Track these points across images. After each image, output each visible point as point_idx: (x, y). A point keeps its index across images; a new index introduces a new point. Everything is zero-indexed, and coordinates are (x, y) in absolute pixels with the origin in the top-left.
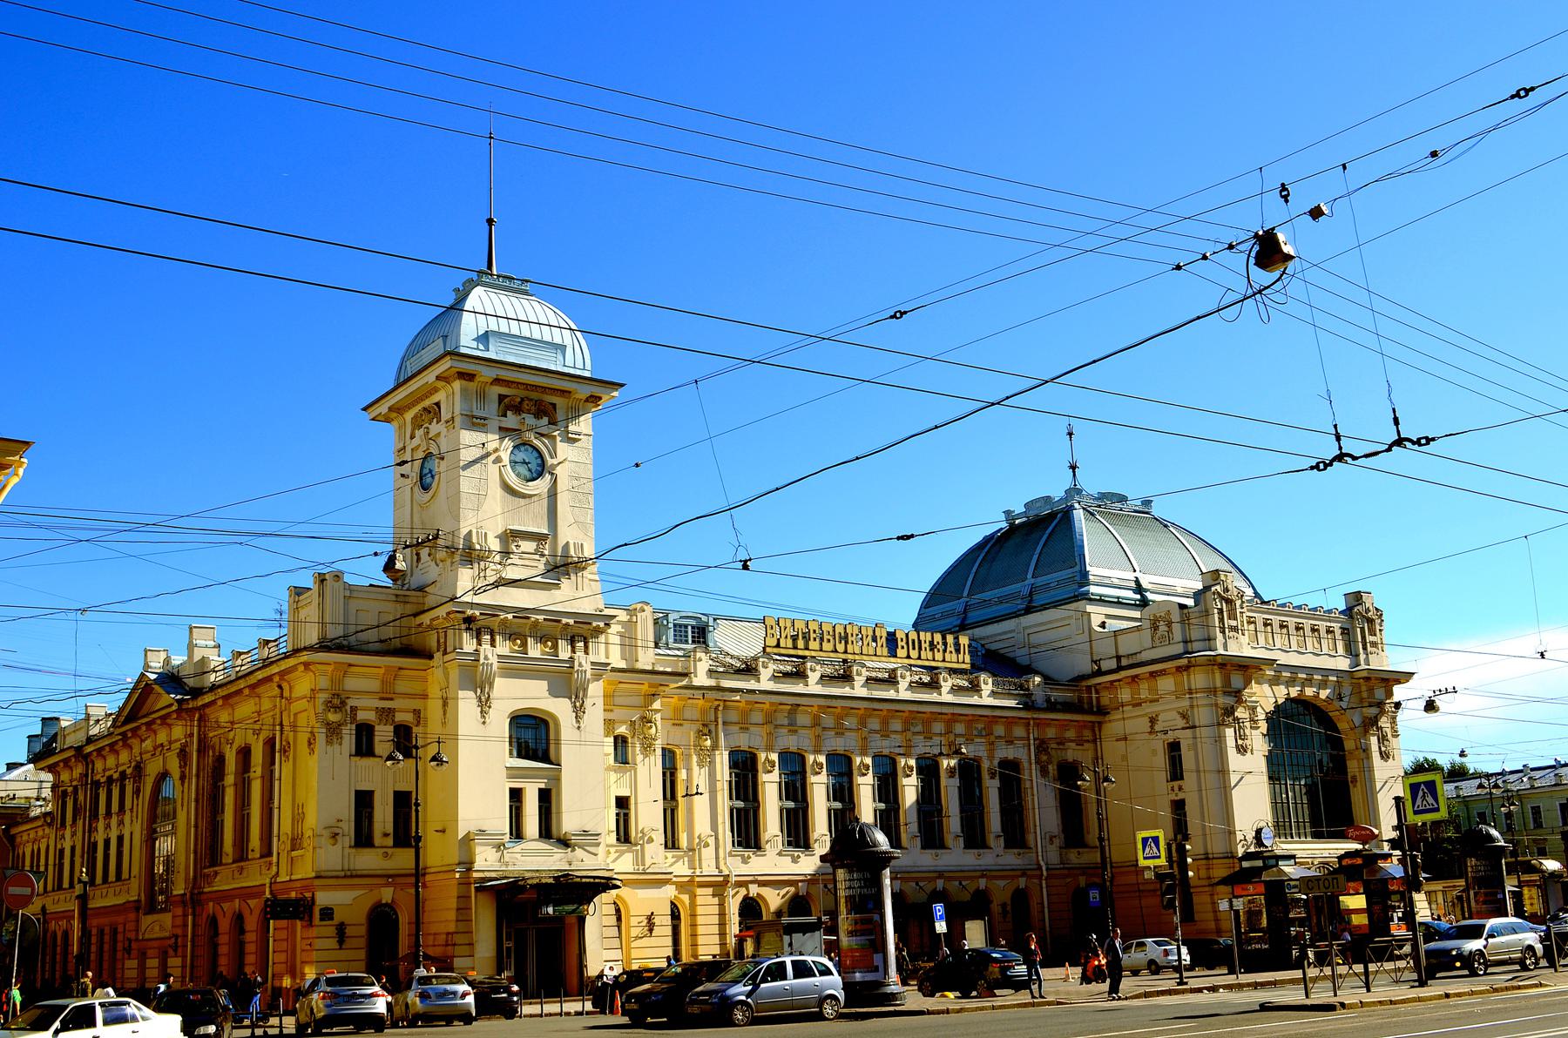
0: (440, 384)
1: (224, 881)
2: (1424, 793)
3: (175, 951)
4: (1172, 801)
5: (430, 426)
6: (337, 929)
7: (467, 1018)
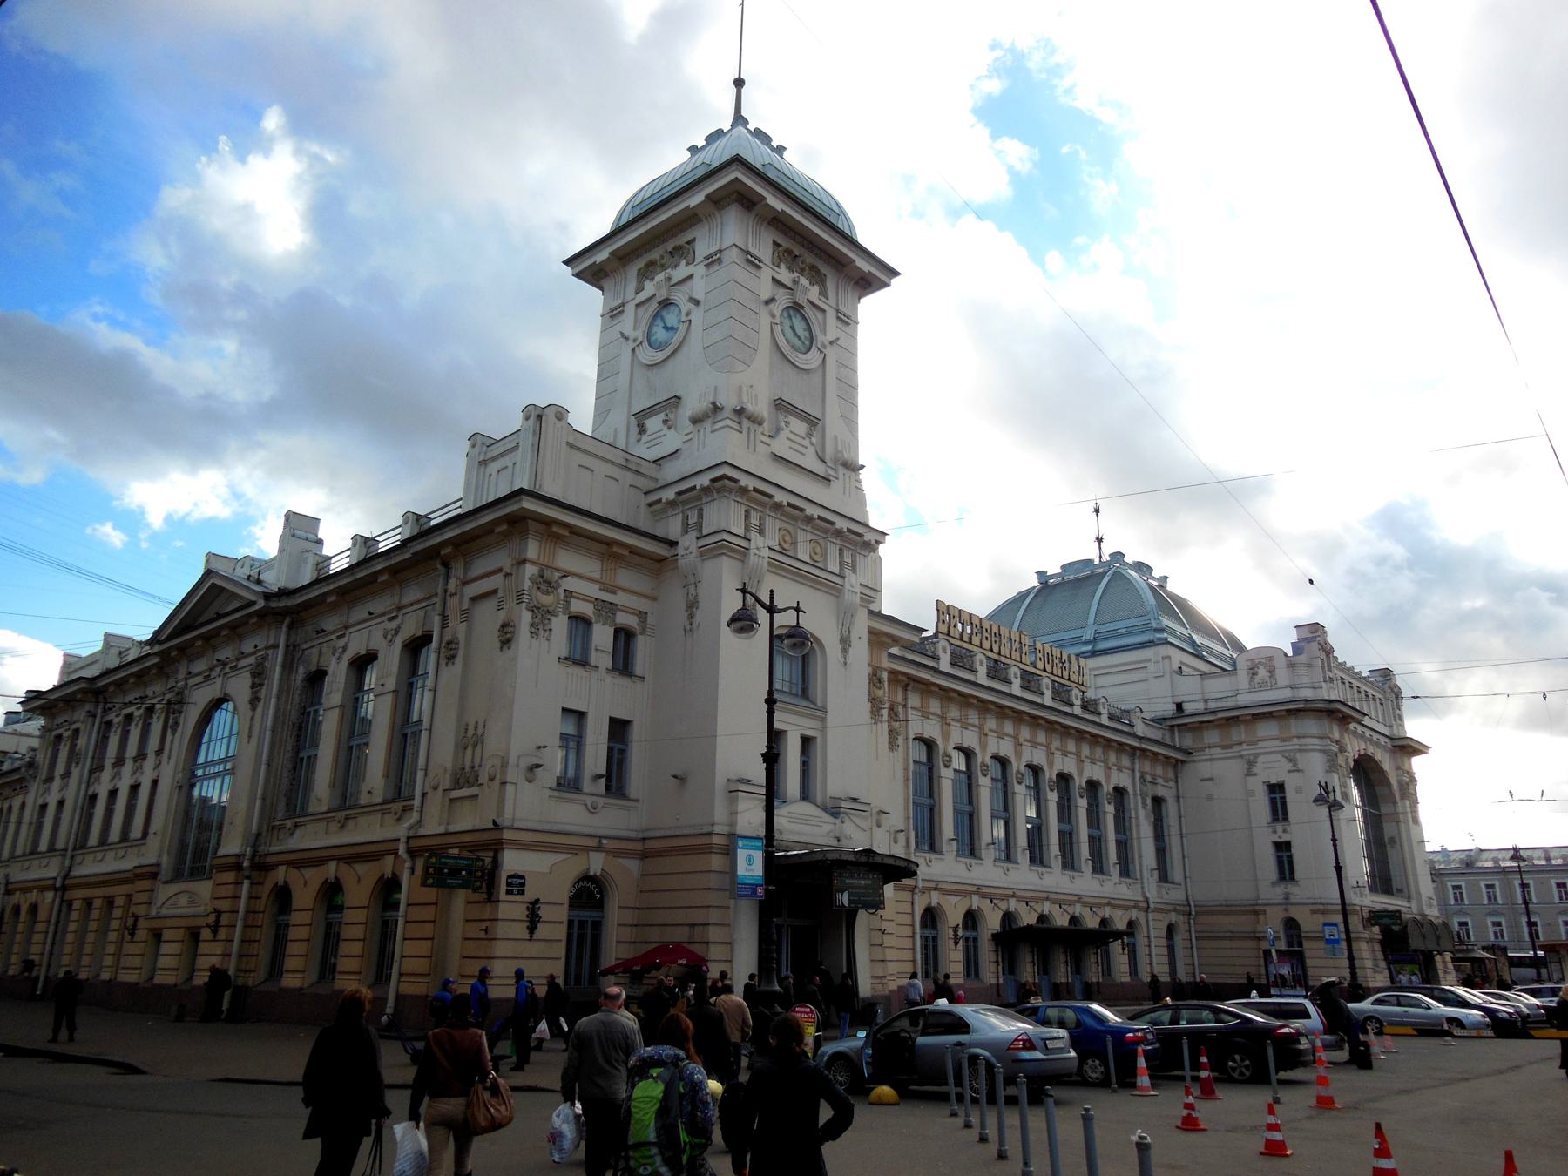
3: (215, 932)
6: (528, 908)
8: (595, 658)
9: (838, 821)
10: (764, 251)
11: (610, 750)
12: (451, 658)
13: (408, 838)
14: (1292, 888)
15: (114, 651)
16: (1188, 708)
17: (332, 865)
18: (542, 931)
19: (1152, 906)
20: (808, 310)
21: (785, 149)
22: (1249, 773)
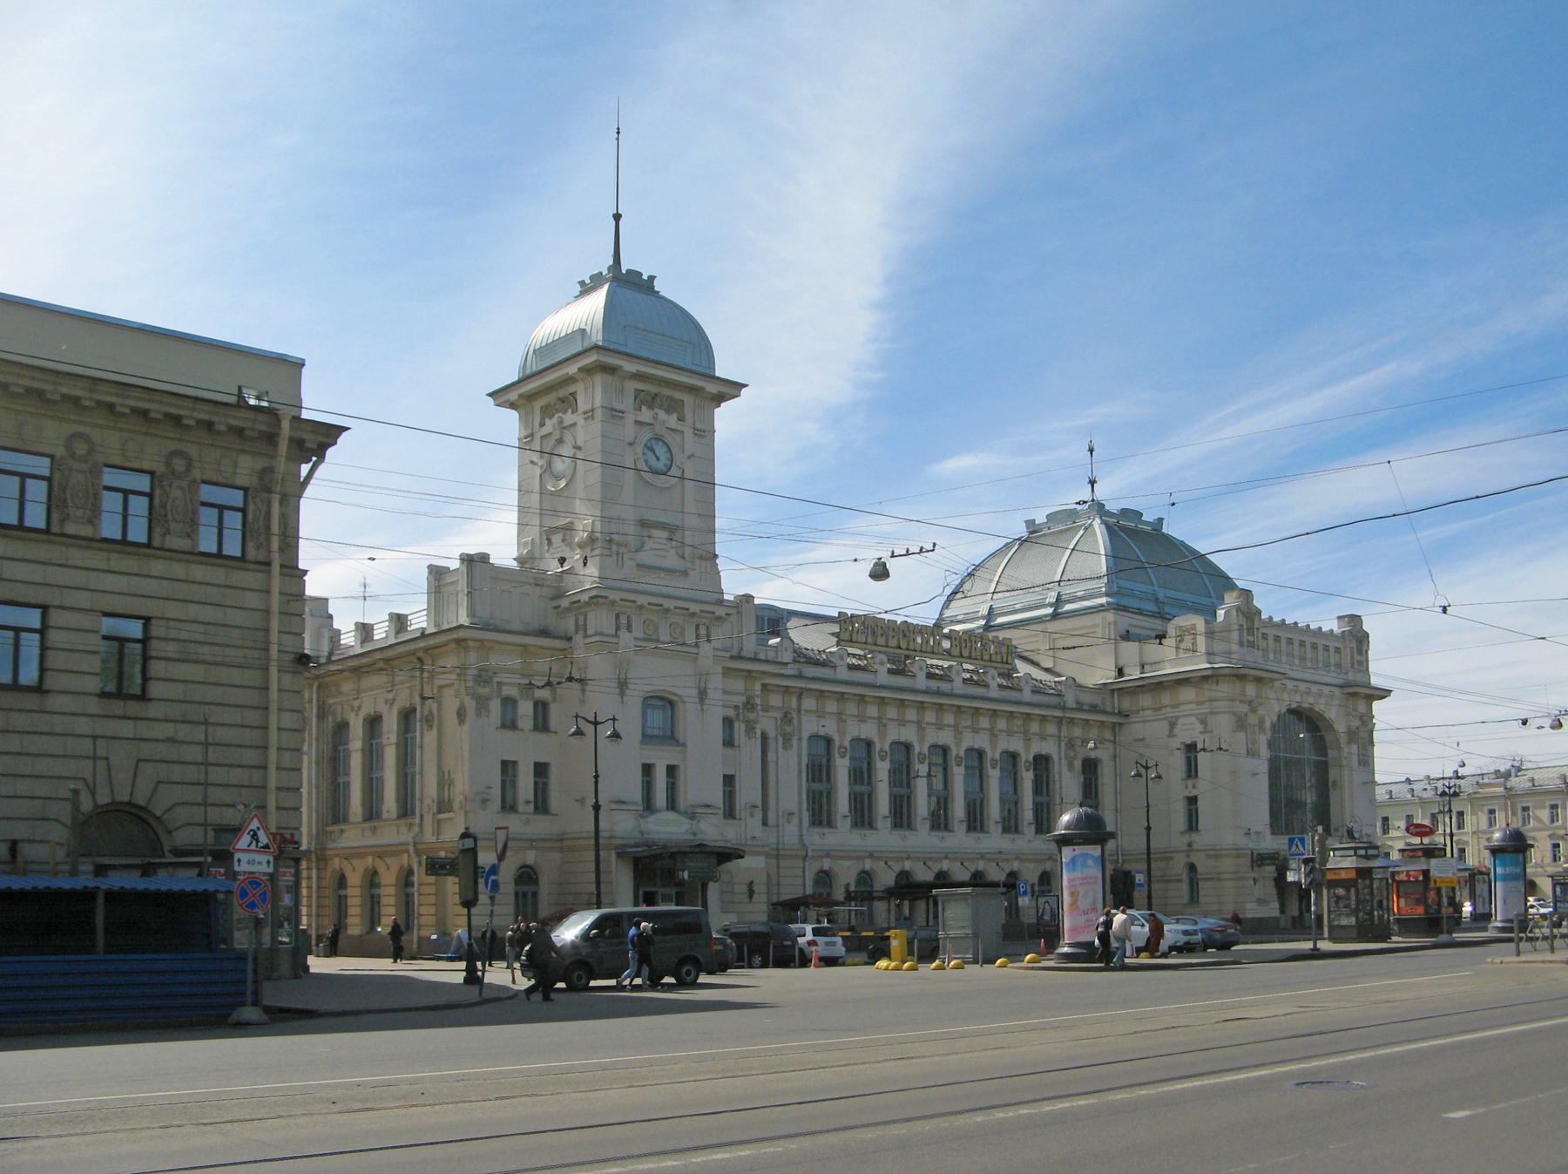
1: (352, 836)
5: (564, 416)
8: (520, 724)
11: (536, 783)
14: (1195, 837)
17: (370, 858)
20: (669, 438)
21: (655, 277)
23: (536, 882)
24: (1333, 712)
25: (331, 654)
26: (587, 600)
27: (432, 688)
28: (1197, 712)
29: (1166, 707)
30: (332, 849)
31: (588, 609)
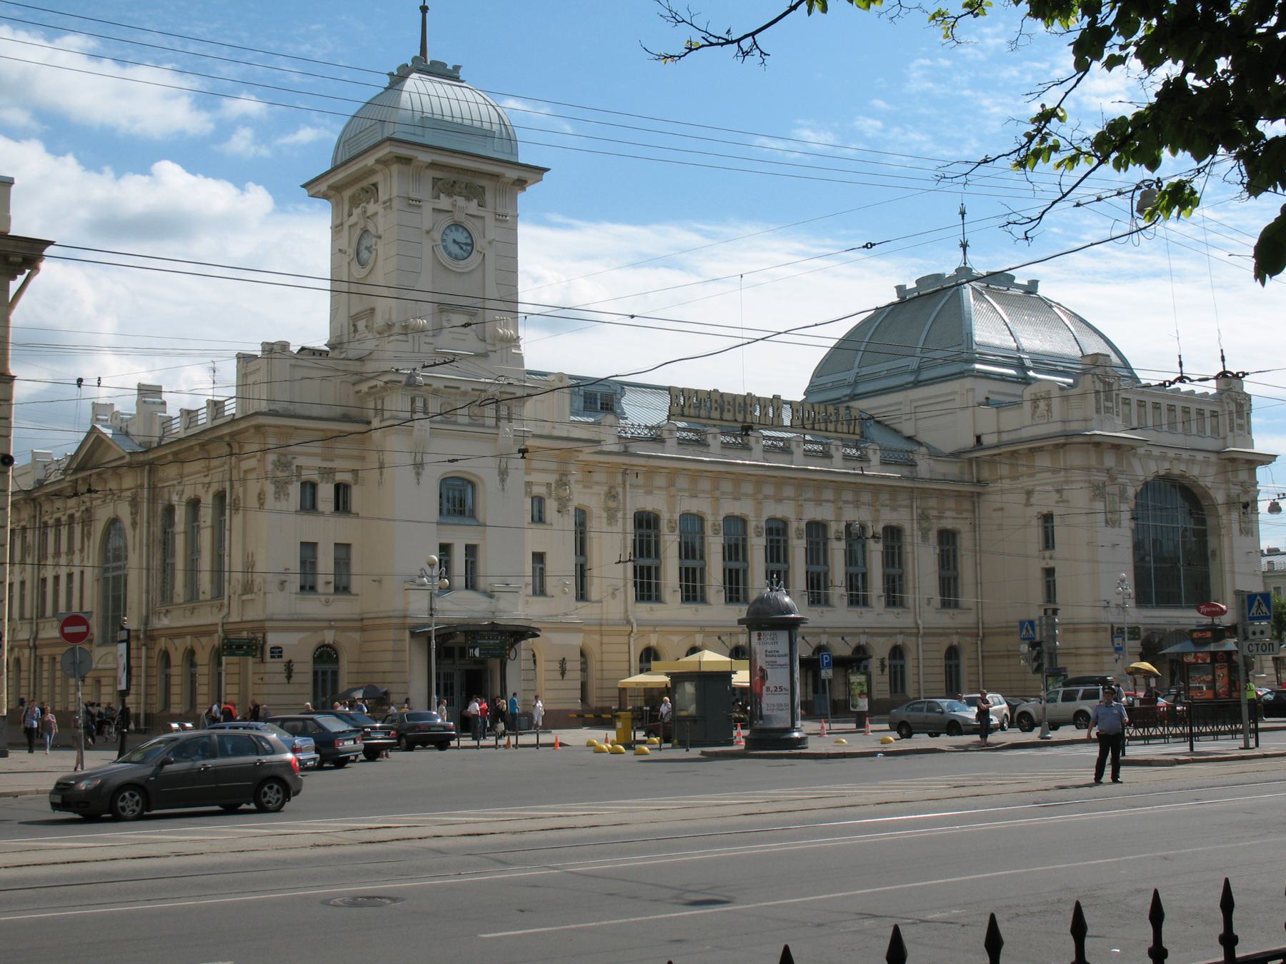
0: (378, 167)
2: (1259, 603)
4: (1043, 568)
7: (442, 742)
9: (493, 600)
10: (424, 191)
12: (237, 510)
13: (223, 624)
15: (41, 466)
16: (987, 440)
18: (295, 678)
19: (921, 631)
20: (469, 224)
22: (1028, 504)
23: (336, 661)
24: (1207, 477)
25: (161, 439)
26: (366, 390)
27: (239, 472)
28: (1052, 480)
29: (1023, 476)
30: (42, 639)
31: (385, 394)
